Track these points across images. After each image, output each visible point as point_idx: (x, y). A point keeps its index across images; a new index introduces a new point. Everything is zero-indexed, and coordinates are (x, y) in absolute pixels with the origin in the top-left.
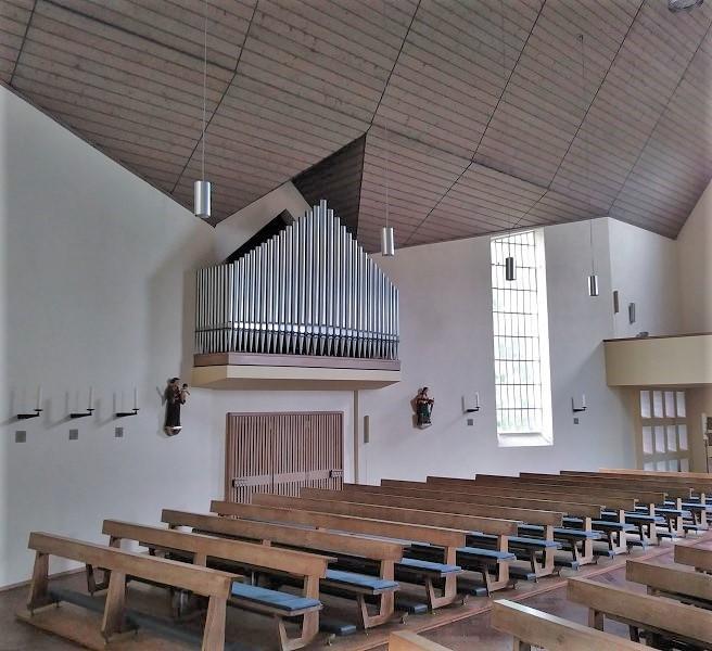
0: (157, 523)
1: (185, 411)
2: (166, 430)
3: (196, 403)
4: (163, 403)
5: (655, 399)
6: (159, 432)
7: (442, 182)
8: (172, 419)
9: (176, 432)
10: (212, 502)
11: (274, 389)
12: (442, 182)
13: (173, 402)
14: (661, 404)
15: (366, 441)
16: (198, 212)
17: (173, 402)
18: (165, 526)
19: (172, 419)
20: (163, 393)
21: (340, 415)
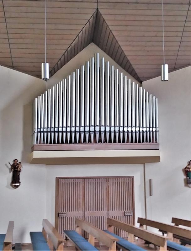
0: (169, 222)
1: (22, 176)
2: (11, 185)
3: (26, 171)
4: (10, 172)
5: (121, 61)
6: (7, 187)
7: (179, 19)
8: (16, 179)
9: (17, 187)
10: (138, 218)
11: (93, 165)
12: (179, 19)
13: (15, 170)
14: (108, 42)
15: (151, 195)
16: (43, 77)
17: (15, 170)
18: (173, 225)
19: (16, 179)
20: (10, 167)
21: (132, 178)
